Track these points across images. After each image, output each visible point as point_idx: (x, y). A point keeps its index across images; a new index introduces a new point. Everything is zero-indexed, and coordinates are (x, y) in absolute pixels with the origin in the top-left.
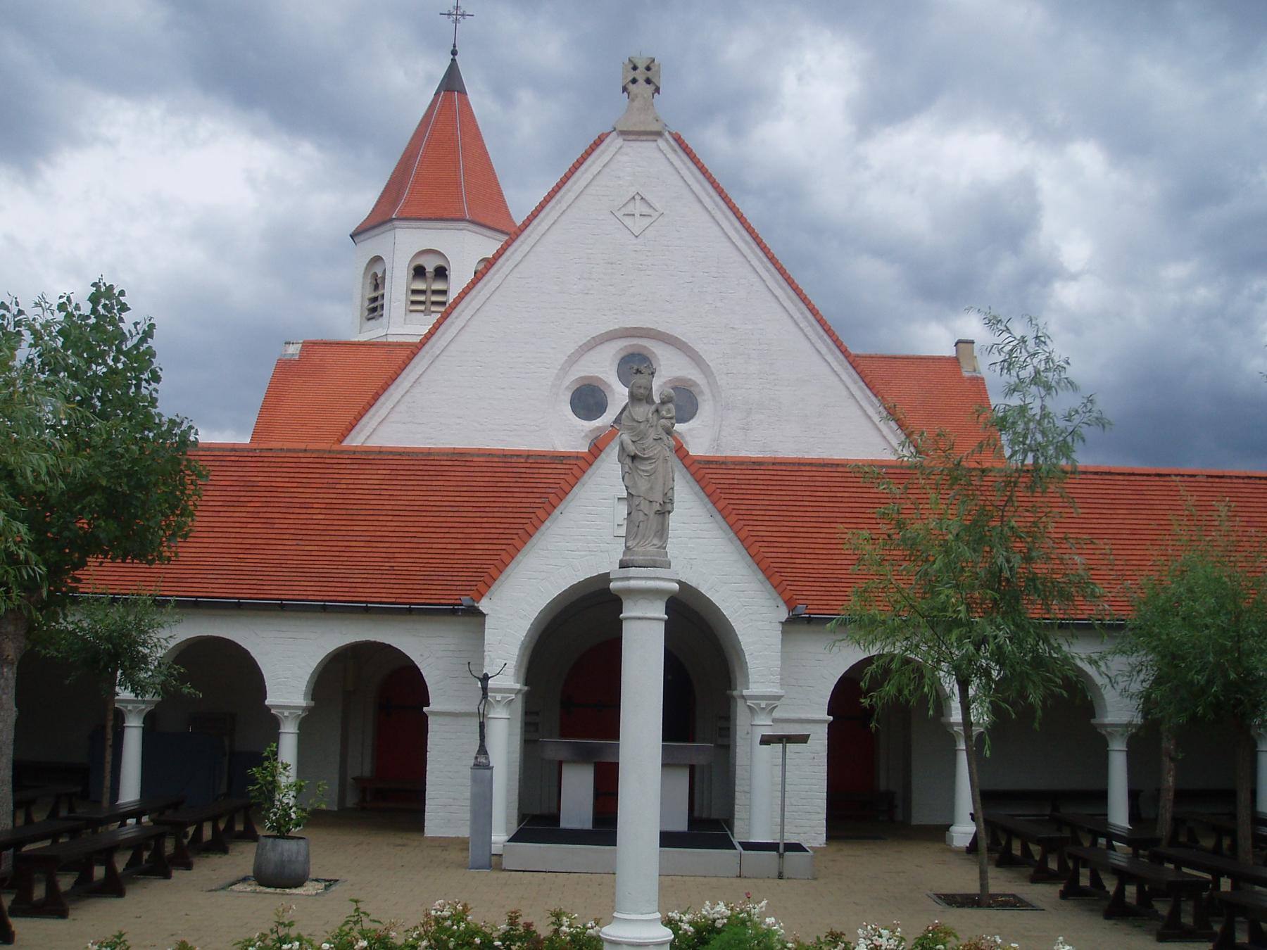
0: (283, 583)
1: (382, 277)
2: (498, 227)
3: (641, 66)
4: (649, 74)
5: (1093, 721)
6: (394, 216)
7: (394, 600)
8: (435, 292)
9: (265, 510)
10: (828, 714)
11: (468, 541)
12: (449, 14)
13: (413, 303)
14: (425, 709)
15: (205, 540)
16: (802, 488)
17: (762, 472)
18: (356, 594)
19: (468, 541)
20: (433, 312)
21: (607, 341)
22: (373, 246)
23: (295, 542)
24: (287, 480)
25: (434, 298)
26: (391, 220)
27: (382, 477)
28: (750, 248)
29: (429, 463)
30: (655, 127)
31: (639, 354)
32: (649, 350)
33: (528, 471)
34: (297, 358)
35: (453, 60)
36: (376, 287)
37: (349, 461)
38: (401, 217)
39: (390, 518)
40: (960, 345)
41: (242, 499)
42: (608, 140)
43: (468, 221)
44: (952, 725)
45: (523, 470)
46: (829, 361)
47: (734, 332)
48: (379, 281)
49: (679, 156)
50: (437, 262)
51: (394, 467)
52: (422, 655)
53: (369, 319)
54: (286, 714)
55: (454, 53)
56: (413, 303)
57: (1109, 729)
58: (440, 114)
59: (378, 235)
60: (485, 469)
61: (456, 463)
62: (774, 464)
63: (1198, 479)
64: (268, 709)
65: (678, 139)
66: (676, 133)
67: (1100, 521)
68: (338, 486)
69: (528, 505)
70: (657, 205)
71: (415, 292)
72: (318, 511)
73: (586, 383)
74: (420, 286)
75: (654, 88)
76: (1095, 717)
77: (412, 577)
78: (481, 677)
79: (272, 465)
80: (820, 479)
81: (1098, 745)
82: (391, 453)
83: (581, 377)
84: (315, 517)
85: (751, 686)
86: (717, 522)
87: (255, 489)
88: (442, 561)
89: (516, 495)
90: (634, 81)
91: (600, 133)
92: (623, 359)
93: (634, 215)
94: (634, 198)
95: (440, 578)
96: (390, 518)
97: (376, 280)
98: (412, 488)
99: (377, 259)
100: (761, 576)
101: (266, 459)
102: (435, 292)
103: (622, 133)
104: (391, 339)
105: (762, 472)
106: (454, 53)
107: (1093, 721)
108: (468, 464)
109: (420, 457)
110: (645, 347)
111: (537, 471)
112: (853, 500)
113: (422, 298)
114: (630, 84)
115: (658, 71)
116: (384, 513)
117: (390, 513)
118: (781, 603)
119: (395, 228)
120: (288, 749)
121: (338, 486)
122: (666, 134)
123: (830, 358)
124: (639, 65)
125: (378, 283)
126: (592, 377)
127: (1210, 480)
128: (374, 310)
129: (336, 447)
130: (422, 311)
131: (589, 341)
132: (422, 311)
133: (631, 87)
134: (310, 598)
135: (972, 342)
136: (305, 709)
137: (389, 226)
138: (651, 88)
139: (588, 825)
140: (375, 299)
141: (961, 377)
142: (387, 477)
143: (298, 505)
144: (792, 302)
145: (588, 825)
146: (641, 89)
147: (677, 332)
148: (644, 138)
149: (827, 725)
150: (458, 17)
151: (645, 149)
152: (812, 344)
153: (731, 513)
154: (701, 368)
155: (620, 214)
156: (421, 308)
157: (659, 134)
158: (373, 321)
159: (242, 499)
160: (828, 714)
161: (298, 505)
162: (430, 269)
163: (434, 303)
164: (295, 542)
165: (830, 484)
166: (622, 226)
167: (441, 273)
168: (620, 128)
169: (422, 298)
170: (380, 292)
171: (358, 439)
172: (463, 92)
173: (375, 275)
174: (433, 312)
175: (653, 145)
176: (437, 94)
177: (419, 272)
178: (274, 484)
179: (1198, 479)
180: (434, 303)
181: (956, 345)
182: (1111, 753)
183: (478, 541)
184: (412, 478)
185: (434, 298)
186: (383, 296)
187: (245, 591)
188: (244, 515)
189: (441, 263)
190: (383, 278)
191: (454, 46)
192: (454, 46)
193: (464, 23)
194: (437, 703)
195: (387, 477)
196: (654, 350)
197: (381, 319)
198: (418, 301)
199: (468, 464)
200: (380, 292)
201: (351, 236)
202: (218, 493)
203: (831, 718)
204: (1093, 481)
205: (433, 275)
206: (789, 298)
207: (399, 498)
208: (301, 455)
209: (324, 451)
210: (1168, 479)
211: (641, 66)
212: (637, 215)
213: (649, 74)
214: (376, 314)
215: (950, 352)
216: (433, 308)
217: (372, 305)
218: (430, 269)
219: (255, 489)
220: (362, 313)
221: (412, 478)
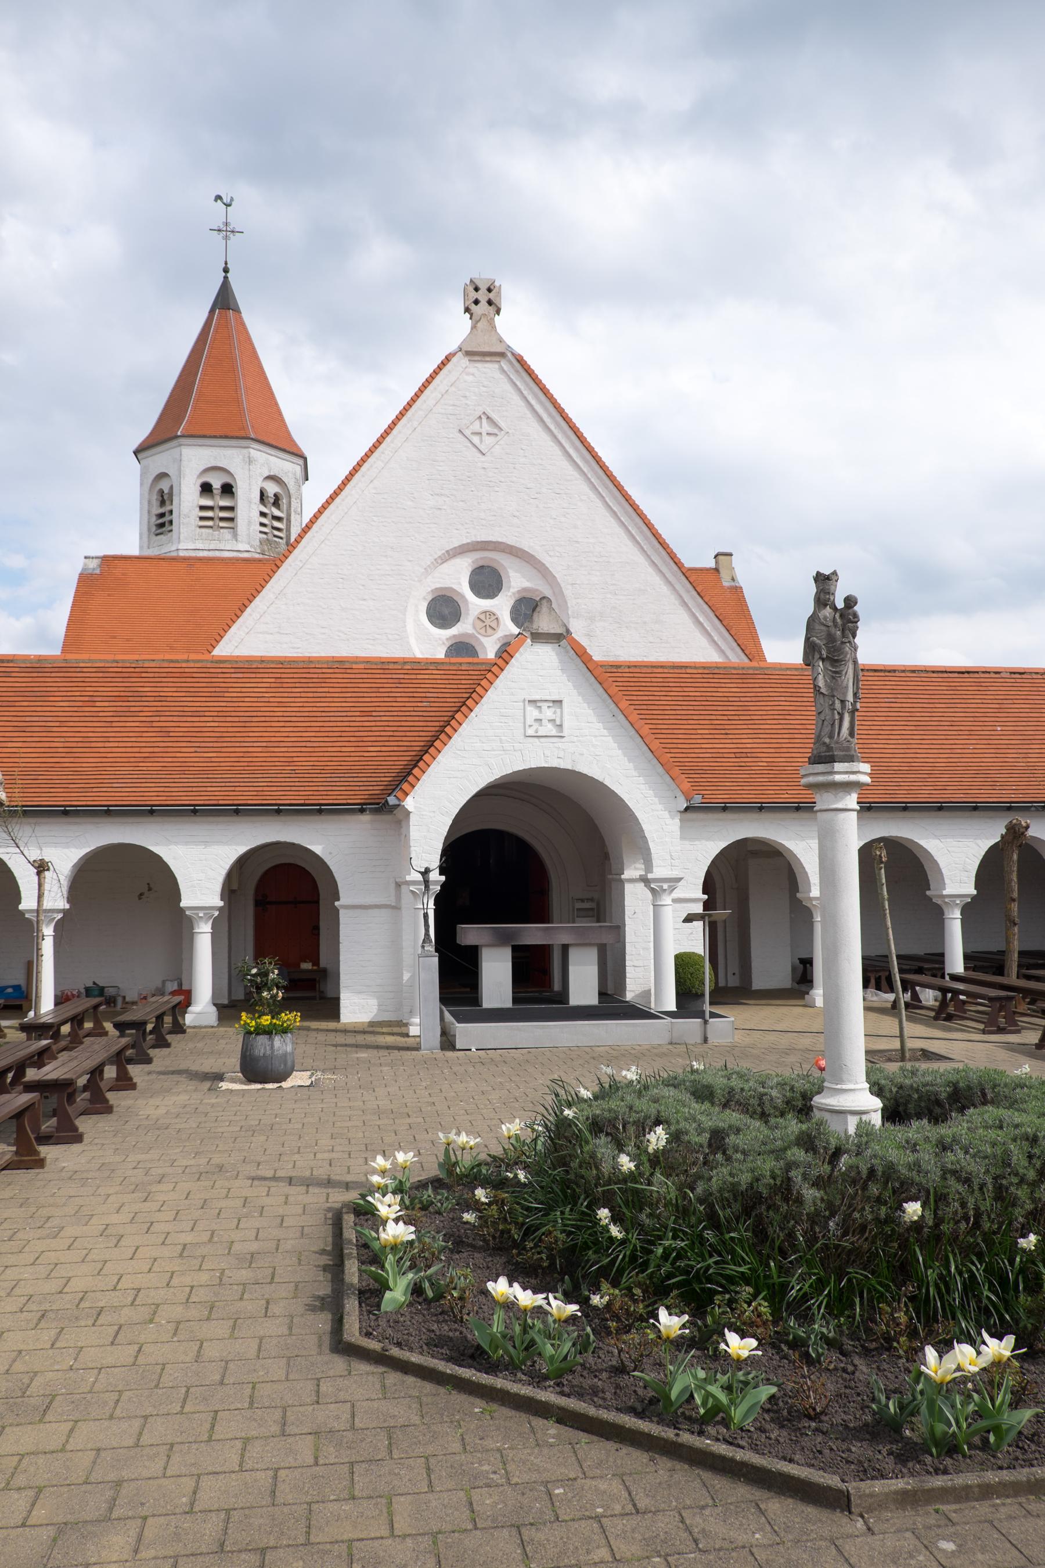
0: (190, 789)
1: (168, 493)
2: (280, 446)
3: (483, 288)
4: (491, 296)
5: (928, 893)
6: (179, 433)
7: (302, 802)
8: (222, 508)
9: (158, 719)
10: (703, 893)
11: (360, 744)
12: (233, 232)
13: (202, 518)
14: (336, 903)
15: (102, 750)
16: (658, 689)
17: (620, 675)
18: (264, 798)
19: (360, 744)
20: (222, 528)
21: (460, 554)
22: (160, 460)
23: (193, 750)
24: (175, 689)
25: (223, 514)
26: (177, 437)
27: (268, 685)
28: (590, 466)
29: (312, 671)
30: (499, 349)
31: (488, 567)
32: (499, 562)
33: (406, 676)
34: (98, 571)
35: (226, 278)
36: (163, 503)
37: (232, 670)
38: (186, 434)
39: (282, 724)
40: (720, 558)
41: (132, 709)
42: (454, 360)
43: (252, 439)
44: (811, 899)
45: (402, 676)
46: (664, 571)
47: (577, 545)
48: (166, 497)
49: (522, 378)
50: (223, 479)
51: (279, 675)
52: (330, 853)
53: (157, 535)
54: (201, 915)
55: (226, 270)
56: (202, 518)
57: (947, 900)
58: (216, 331)
59: (163, 451)
60: (365, 676)
61: (337, 671)
62: (629, 667)
63: (1002, 675)
64: (182, 911)
65: (520, 360)
66: (519, 355)
67: (923, 714)
68: (226, 695)
69: (412, 709)
70: (502, 424)
71: (202, 508)
72: (211, 719)
73: (440, 594)
74: (208, 502)
75: (496, 309)
76: (929, 889)
77: (314, 780)
78: (423, 870)
79: (157, 675)
80: (673, 680)
81: (936, 914)
82: (273, 662)
83: (436, 589)
84: (208, 724)
85: (655, 870)
86: (618, 721)
87: (144, 699)
88: (339, 763)
89: (399, 699)
90: (476, 302)
91: (448, 353)
92: (473, 571)
93: (481, 434)
94: (480, 417)
95: (342, 779)
96: (282, 724)
97: (162, 496)
98: (298, 695)
99: (163, 476)
100: (660, 769)
101: (149, 670)
102: (222, 508)
103: (468, 353)
104: (182, 554)
105: (620, 675)
106: (226, 270)
107: (928, 893)
108: (348, 671)
109: (301, 665)
110: (495, 560)
111: (414, 676)
112: (704, 699)
113: (210, 514)
114: (473, 305)
115: (499, 293)
116: (276, 719)
117: (281, 719)
118: (679, 794)
119: (180, 445)
120: (886, 904)
121: (226, 695)
122: (509, 355)
123: (664, 569)
124: (480, 286)
125: (165, 498)
126: (446, 588)
127: (1013, 676)
128: (162, 525)
129: (206, 657)
130: (211, 527)
131: (443, 554)
132: (211, 527)
133: (473, 307)
134: (221, 802)
135: (731, 555)
136: (220, 909)
137: (174, 443)
138: (492, 309)
139: (508, 1004)
140: (162, 515)
141: (723, 587)
142: (273, 685)
143: (190, 714)
144: (630, 517)
145: (508, 1004)
146: (483, 308)
147: (525, 544)
148: (488, 359)
149: (702, 904)
150: (228, 233)
151: (490, 369)
152: (648, 556)
153: (632, 713)
154: (547, 580)
155: (467, 432)
156: (210, 523)
157: (502, 355)
158: (161, 536)
159: (132, 709)
160: (703, 893)
161: (190, 714)
162: (217, 485)
163: (222, 519)
164: (193, 750)
165: (682, 685)
166: (469, 445)
167: (228, 489)
168: (464, 349)
169: (210, 514)
170: (167, 508)
171: (222, 650)
172: (237, 310)
173: (161, 492)
174: (222, 528)
175: (496, 366)
176: (212, 311)
177: (206, 489)
178: (162, 694)
179: (1002, 675)
180: (222, 519)
181: (715, 557)
182: (946, 921)
183: (370, 744)
184: (297, 685)
185: (223, 514)
186: (171, 512)
187: (153, 797)
188: (137, 724)
189: (228, 480)
190: (171, 494)
191: (226, 263)
192: (226, 263)
193: (234, 239)
194: (346, 897)
195: (273, 685)
196: (502, 562)
197: (170, 534)
198: (207, 517)
199: (348, 671)
200: (167, 508)
201: (136, 453)
202: (106, 704)
203: (706, 897)
204: (912, 679)
205: (220, 491)
206: (626, 513)
207: (289, 704)
208: (184, 665)
209: (108, 662)
210: (976, 675)
211: (483, 288)
212: (484, 434)
213: (491, 296)
214: (164, 529)
215: (711, 564)
216: (222, 524)
217: (161, 521)
218: (217, 485)
219: (144, 699)
220: (149, 530)
221: (297, 685)
